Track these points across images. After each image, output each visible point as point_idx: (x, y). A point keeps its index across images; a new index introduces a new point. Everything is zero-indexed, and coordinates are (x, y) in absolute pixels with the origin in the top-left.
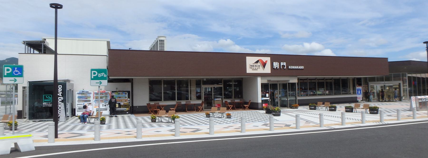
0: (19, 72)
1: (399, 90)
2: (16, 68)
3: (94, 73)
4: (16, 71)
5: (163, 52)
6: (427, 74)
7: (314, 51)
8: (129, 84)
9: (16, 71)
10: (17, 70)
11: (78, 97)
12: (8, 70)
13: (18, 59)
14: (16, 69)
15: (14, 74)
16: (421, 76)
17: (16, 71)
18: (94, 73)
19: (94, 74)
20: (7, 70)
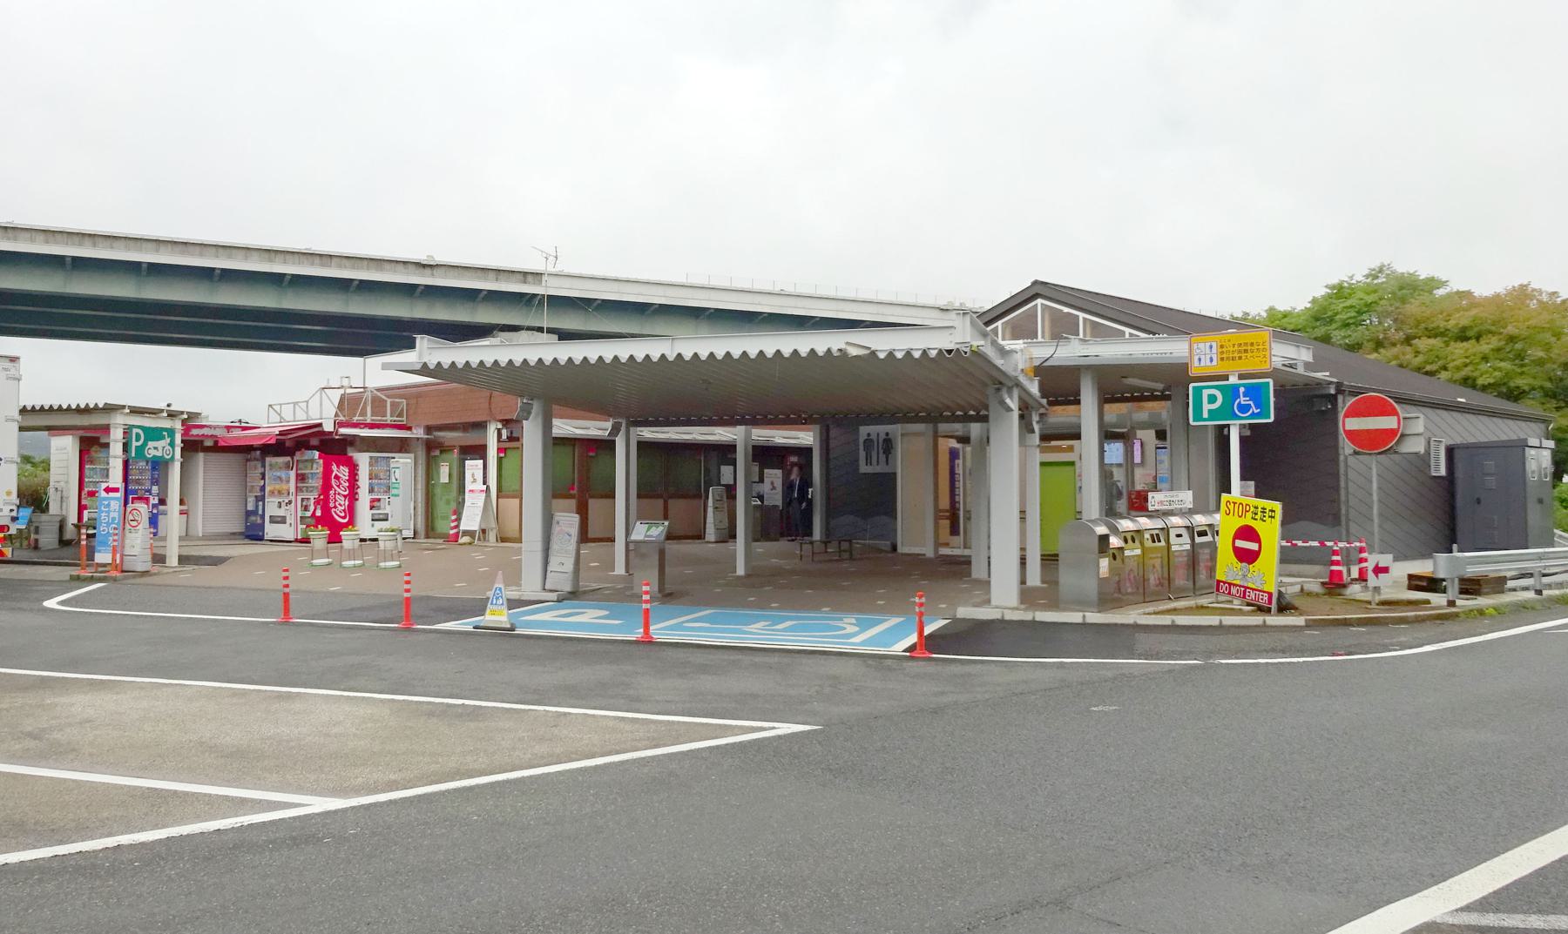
0: (1252, 405)
1: (198, 537)
2: (1242, 390)
3: (1209, 395)
4: (1243, 403)
5: (94, 552)
6: (1564, 918)
7: (677, 544)
8: (757, 479)
9: (1243, 400)
10: (1244, 396)
11: (1043, 464)
12: (1212, 399)
13: (796, 350)
14: (1241, 395)
15: (1235, 413)
16: (116, 441)
17: (1243, 400)
18: (1209, 395)
19: (1209, 403)
20: (286, 520)
